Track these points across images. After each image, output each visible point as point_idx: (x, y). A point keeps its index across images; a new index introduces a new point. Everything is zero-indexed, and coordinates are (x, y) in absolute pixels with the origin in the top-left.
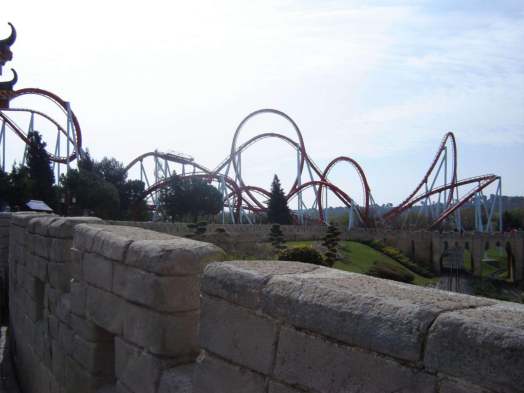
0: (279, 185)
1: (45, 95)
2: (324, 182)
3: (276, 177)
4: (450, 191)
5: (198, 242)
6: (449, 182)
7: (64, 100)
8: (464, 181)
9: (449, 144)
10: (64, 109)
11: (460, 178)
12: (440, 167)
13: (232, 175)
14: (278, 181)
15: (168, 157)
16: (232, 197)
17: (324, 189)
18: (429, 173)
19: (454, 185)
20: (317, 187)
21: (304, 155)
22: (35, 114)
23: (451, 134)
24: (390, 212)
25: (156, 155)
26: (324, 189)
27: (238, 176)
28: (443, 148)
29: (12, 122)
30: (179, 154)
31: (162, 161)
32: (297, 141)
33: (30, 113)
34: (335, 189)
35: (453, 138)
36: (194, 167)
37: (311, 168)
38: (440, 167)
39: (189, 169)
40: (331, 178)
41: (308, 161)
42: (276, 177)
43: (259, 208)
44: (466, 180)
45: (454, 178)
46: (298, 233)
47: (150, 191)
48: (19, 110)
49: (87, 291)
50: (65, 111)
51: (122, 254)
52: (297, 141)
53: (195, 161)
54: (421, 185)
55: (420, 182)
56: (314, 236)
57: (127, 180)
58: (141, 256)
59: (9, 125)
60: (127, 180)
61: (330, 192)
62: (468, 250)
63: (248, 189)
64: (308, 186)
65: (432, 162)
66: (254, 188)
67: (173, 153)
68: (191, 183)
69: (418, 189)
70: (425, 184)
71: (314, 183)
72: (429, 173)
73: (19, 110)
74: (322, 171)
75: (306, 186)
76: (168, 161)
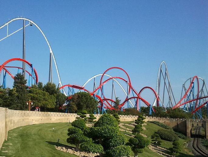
2: (138, 98)
7: (30, 63)
9: (195, 81)
13: (100, 95)
17: (139, 100)
19: (199, 98)
20: (136, 99)
21: (130, 87)
23: (196, 77)
25: (69, 86)
26: (139, 100)
27: (102, 94)
31: (71, 88)
32: (127, 80)
34: (142, 100)
37: (133, 91)
39: (82, 91)
40: (142, 96)
41: (132, 88)
52: (127, 80)
57: (43, 86)
60: (43, 86)
61: (141, 101)
63: (105, 99)
66: (108, 99)
71: (134, 97)
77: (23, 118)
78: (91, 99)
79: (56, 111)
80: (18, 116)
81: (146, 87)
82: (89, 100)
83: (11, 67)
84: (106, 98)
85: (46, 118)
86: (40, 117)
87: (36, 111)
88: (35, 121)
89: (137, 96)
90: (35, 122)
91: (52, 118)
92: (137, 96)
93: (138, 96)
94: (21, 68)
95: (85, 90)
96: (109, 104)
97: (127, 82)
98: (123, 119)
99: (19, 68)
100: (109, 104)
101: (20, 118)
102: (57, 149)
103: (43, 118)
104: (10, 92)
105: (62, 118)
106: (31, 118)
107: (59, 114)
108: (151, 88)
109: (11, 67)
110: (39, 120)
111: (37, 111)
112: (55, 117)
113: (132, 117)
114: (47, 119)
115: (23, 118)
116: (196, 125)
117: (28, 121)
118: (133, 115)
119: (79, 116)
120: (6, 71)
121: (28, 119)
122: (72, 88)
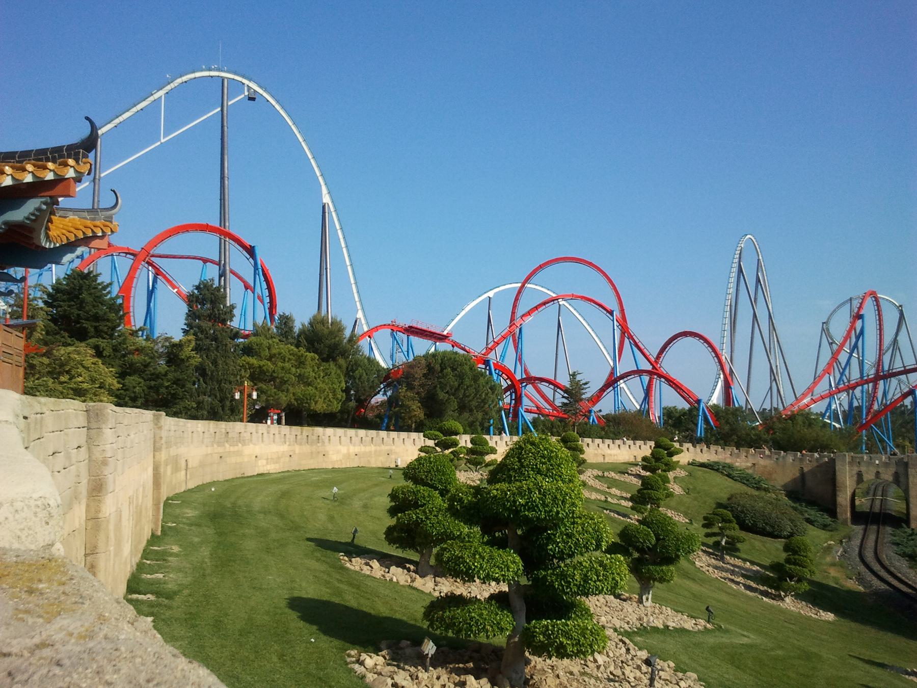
2: (655, 373)
5: (745, 487)
6: (871, 372)
7: (248, 242)
9: (869, 310)
10: (248, 257)
15: (412, 331)
16: (509, 393)
17: (656, 382)
20: (646, 378)
21: (625, 331)
22: (208, 264)
23: (873, 294)
25: (394, 328)
27: (519, 359)
29: (167, 275)
32: (613, 305)
33: (201, 262)
40: (668, 365)
41: (631, 337)
43: (861, 589)
46: (609, 451)
49: (85, 560)
50: (251, 260)
52: (613, 305)
59: (163, 280)
61: (666, 388)
62: (898, 485)
63: (531, 380)
66: (542, 380)
69: (148, 276)
70: (827, 375)
71: (639, 372)
74: (653, 352)
75: (627, 377)
76: (411, 337)
77: (220, 450)
78: (477, 376)
80: (203, 442)
81: (685, 334)
82: (467, 382)
83: (174, 257)
84: (534, 373)
85: (306, 448)
86: (285, 448)
87: (269, 422)
88: (264, 462)
90: (264, 467)
92: (650, 368)
93: (654, 368)
94: (213, 262)
95: (455, 344)
98: (596, 455)
99: (205, 261)
101: (209, 450)
104: (173, 353)
105: (368, 449)
106: (251, 450)
107: (357, 436)
111: (272, 423)
112: (340, 447)
114: (312, 453)
115: (220, 450)
116: (873, 477)
119: (431, 443)
120: (158, 272)
121: (239, 454)
122: (405, 337)
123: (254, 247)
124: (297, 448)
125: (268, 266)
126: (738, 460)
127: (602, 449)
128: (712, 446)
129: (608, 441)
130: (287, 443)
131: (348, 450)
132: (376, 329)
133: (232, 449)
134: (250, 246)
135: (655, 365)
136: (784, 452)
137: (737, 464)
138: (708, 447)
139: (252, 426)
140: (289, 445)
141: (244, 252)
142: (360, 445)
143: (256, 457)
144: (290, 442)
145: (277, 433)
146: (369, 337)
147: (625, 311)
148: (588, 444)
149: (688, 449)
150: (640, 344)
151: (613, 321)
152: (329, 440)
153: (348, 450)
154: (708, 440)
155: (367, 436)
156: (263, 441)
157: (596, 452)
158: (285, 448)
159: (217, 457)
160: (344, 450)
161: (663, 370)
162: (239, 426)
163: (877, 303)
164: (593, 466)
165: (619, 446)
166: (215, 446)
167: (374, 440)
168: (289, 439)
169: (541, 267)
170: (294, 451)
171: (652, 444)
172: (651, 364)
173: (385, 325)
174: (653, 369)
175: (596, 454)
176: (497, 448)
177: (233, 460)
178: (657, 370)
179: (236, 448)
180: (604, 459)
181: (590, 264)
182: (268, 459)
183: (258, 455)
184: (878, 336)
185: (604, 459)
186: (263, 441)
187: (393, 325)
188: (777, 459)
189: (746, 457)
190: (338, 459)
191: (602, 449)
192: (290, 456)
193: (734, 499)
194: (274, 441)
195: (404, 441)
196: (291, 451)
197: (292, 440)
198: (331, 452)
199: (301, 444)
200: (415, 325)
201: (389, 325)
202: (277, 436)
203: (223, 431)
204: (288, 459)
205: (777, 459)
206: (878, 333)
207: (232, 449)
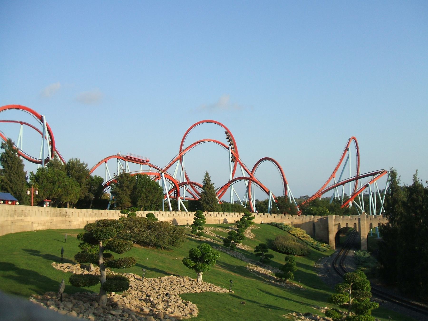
0: (210, 181)
1: (25, 111)
2: (251, 179)
3: (207, 174)
4: (355, 182)
7: (40, 114)
8: (366, 174)
10: (40, 121)
11: (361, 173)
12: (345, 164)
14: (209, 178)
18: (336, 170)
19: (357, 178)
23: (354, 139)
24: (73, 208)
25: (118, 157)
28: (347, 149)
30: (137, 157)
33: (20, 124)
35: (181, 149)
36: (150, 166)
38: (345, 164)
40: (257, 175)
42: (207, 174)
44: (363, 175)
45: (358, 173)
47: (106, 186)
48: (10, 121)
50: (42, 123)
51: (35, 230)
53: (151, 162)
54: (330, 179)
55: (329, 176)
56: (87, 222)
57: (3, 168)
58: (406, 214)
64: (236, 181)
65: (338, 160)
67: (132, 156)
68: (136, 178)
72: (336, 170)
73: (10, 121)
74: (250, 169)
77: (12, 219)
79: (22, 204)
83: (6, 121)
84: (191, 180)
85: (60, 219)
86: (48, 218)
87: (45, 206)
89: (249, 176)
91: (72, 219)
92: (249, 176)
93: (251, 176)
95: (151, 166)
96: (196, 191)
97: (229, 149)
98: (215, 220)
100: (196, 191)
101: (6, 219)
102: (54, 269)
103: (55, 220)
106: (29, 219)
107: (87, 212)
108: (273, 160)
109: (6, 121)
110: (45, 223)
111: (47, 206)
113: (164, 215)
117: (23, 224)
118: (214, 211)
123: (43, 116)
124: (55, 219)
125: (50, 126)
126: (285, 220)
127: (218, 217)
128: (272, 214)
129: (216, 213)
130: (49, 216)
131: (83, 219)
132: (109, 158)
133: (19, 218)
134: (41, 116)
135: (251, 174)
136: (321, 216)
137: (284, 222)
138: (270, 215)
139: (36, 208)
140: (51, 217)
141: (38, 119)
142: (89, 217)
143: (32, 222)
144: (51, 215)
145: (43, 210)
146: (105, 162)
147: (180, 148)
148: (211, 215)
149: (261, 216)
150: (243, 164)
151: (229, 152)
152: (72, 214)
153: (83, 219)
154: (273, 211)
155: (93, 212)
156: (35, 214)
157: (215, 219)
158: (48, 218)
159: (10, 222)
160: (81, 219)
161: (255, 178)
162: (29, 208)
163: (356, 143)
164: (209, 225)
165: (227, 215)
166: (9, 217)
167: (97, 214)
168: (50, 214)
169: (195, 125)
170: (53, 220)
171: (243, 214)
172: (249, 174)
173: (113, 156)
174: (250, 177)
175: (215, 220)
176: (158, 218)
177: (20, 224)
178: (252, 178)
179: (20, 218)
180: (219, 222)
181: (219, 124)
182: (39, 223)
183: (33, 222)
184: (357, 159)
185: (219, 222)
186: (35, 214)
187: (118, 156)
188: (303, 219)
189: (288, 218)
190: (77, 224)
191: (218, 217)
192: (51, 222)
193: (162, 224)
194: (42, 215)
195: (113, 215)
196: (51, 220)
197: (52, 214)
198: (73, 220)
199: (57, 216)
200: (129, 156)
201: (116, 156)
202: (43, 212)
203: (14, 209)
204: (49, 224)
205: (303, 219)
206: (357, 157)
207: (19, 218)
